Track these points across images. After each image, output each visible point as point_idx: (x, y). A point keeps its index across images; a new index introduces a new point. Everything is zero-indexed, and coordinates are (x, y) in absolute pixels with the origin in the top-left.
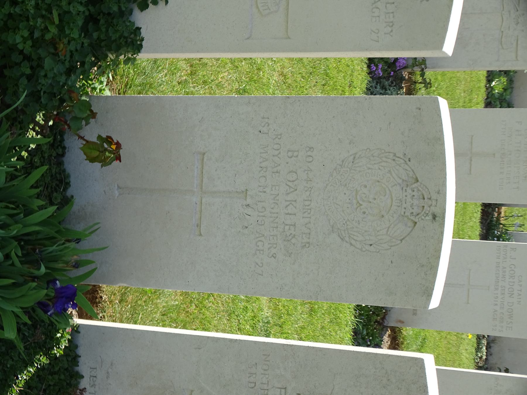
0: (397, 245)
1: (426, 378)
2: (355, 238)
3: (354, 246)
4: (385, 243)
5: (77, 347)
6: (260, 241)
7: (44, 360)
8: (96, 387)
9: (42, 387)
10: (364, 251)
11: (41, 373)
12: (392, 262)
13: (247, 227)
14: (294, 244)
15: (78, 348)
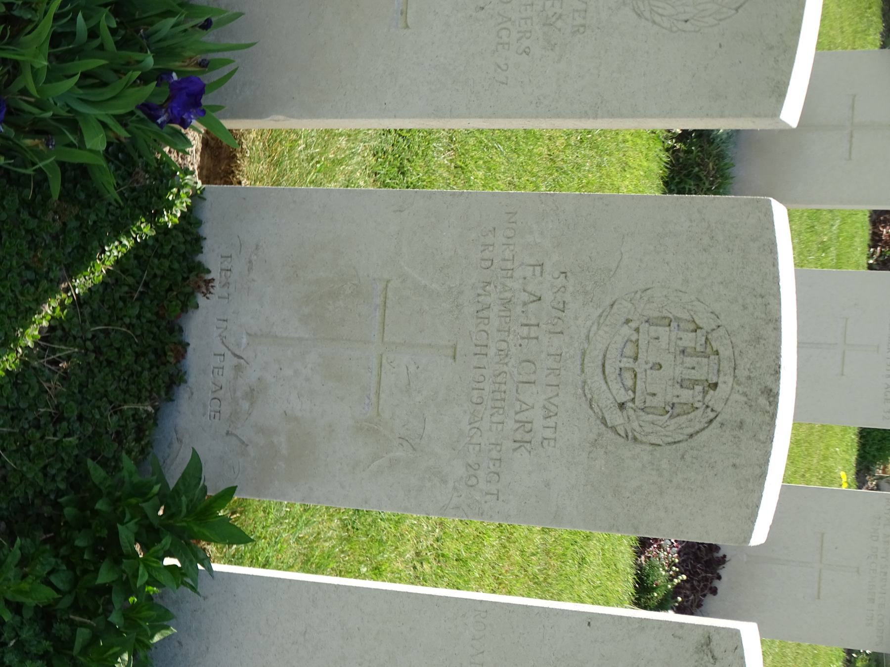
0: (729, 17)
1: (773, 231)
2: (660, 11)
3: (659, 25)
4: (710, 15)
5: (199, 223)
6: (505, 28)
7: (147, 230)
8: (231, 286)
9: (141, 277)
10: (675, 32)
11: (142, 252)
12: (720, 46)
13: (483, 8)
14: (560, 30)
15: (203, 226)
